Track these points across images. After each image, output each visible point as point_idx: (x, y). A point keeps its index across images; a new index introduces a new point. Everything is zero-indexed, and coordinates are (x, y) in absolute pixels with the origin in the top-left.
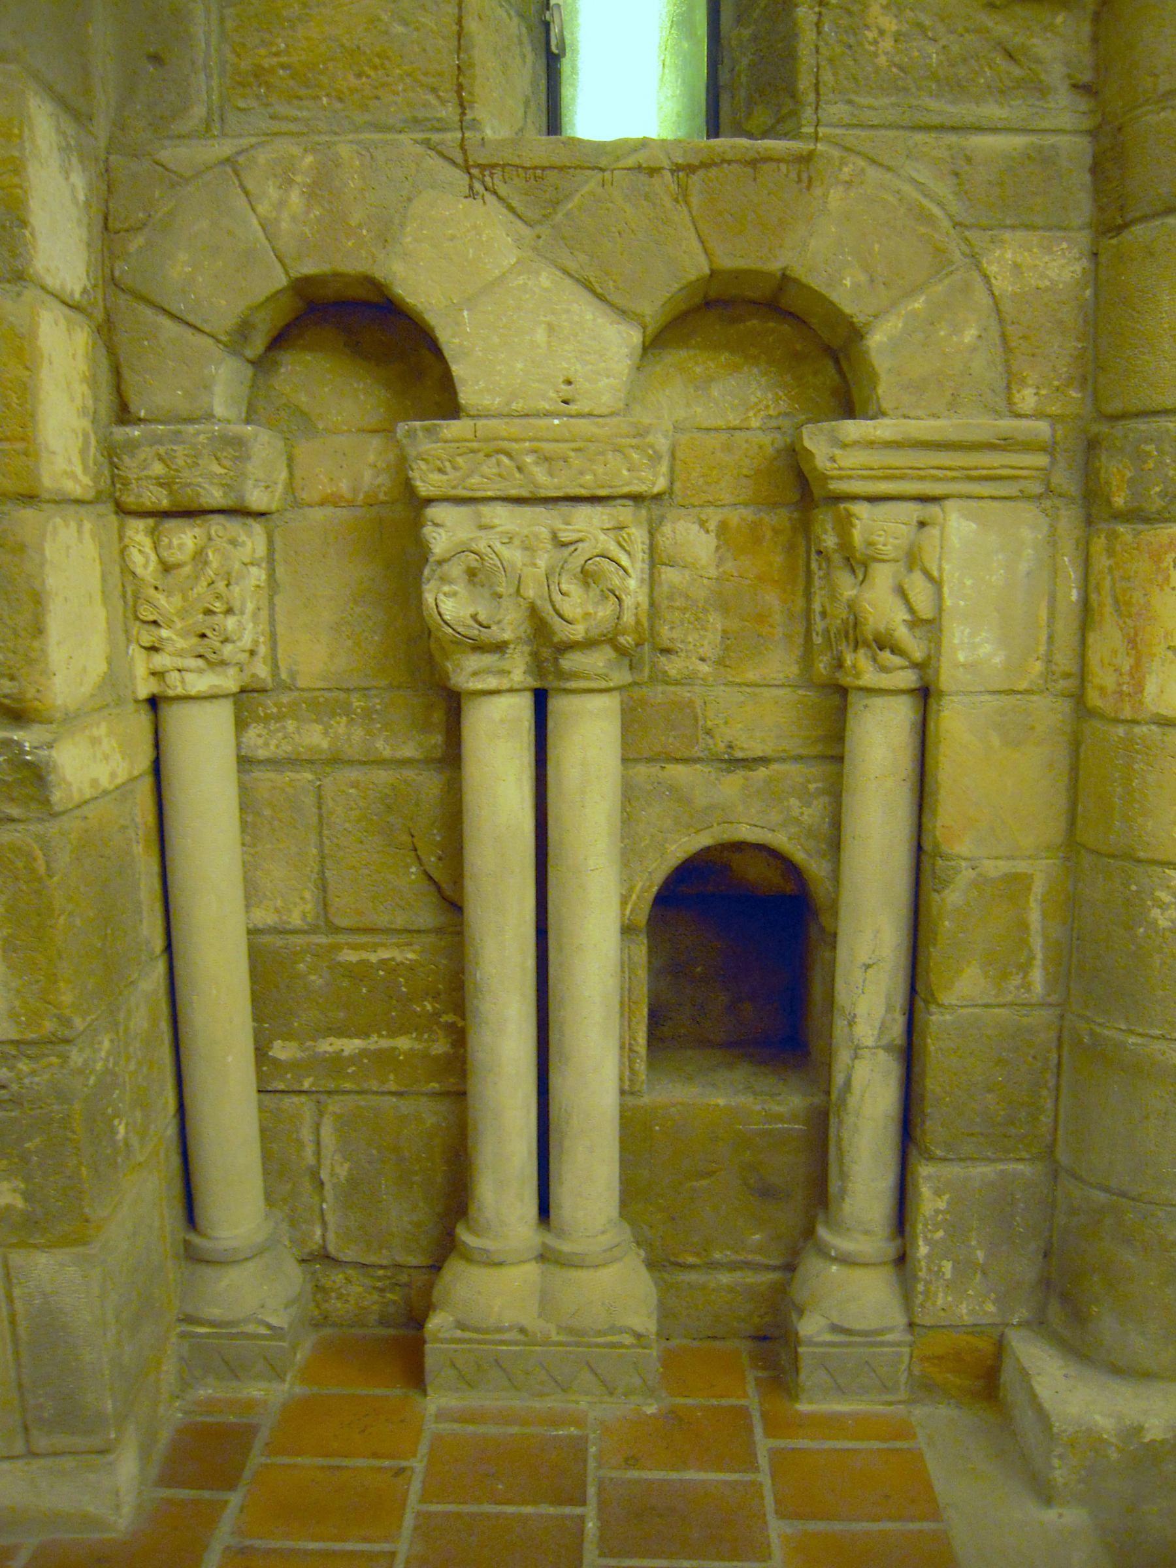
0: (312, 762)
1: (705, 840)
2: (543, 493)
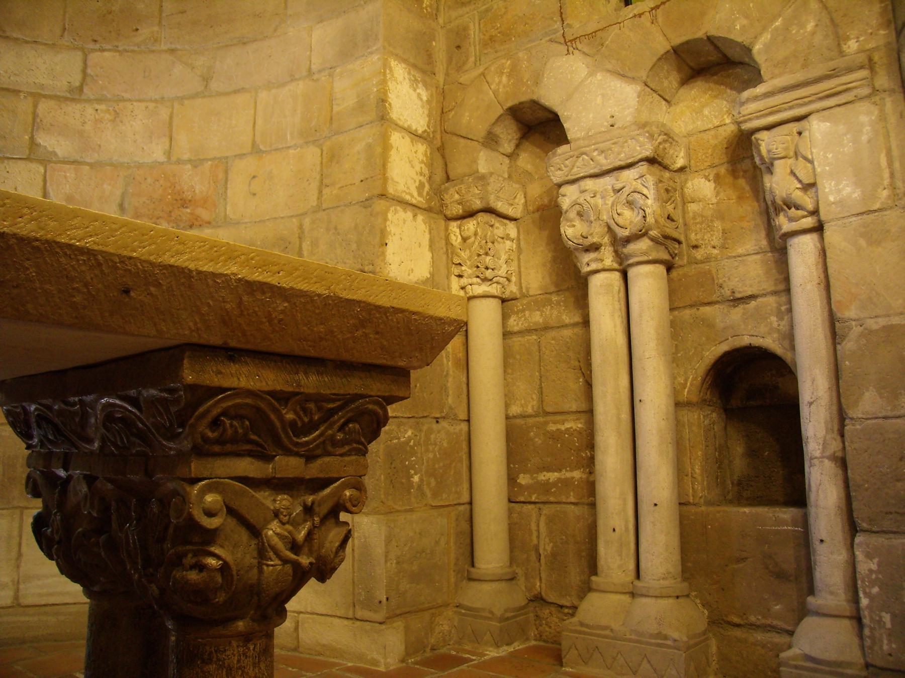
0: (536, 330)
1: (724, 348)
2: (605, 168)
